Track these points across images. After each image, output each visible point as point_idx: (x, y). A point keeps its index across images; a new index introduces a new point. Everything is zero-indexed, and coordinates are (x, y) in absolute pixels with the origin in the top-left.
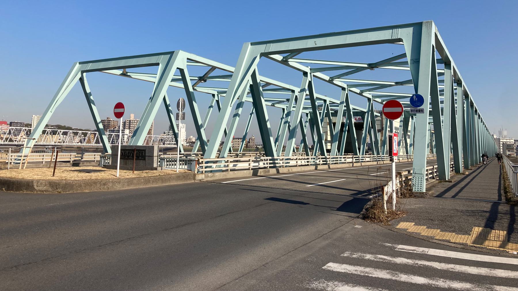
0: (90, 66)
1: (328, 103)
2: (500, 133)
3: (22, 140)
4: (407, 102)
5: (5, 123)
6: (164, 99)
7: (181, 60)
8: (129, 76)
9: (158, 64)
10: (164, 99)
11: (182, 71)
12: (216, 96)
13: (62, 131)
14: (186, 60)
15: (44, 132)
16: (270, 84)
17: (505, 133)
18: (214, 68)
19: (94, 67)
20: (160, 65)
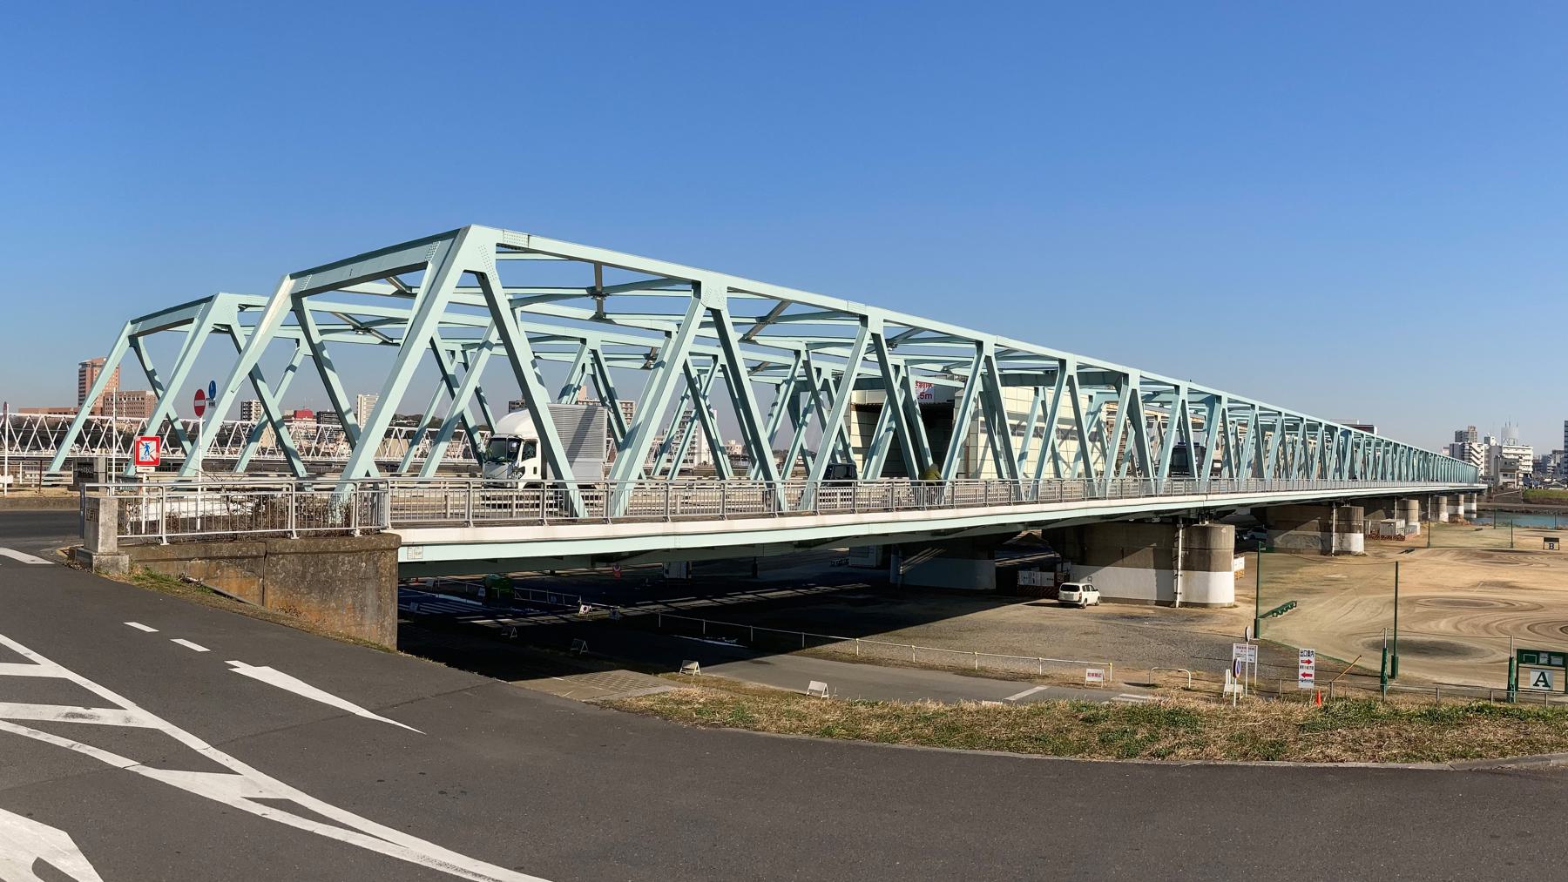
0: (308, 282)
1: (989, 350)
2: (1505, 434)
3: (314, 444)
4: (1446, 453)
5: (307, 414)
6: (686, 366)
7: (480, 247)
8: (610, 321)
9: (423, 266)
10: (686, 366)
11: (716, 313)
12: (902, 370)
13: (405, 429)
14: (494, 248)
15: (388, 434)
16: (923, 330)
17: (1515, 433)
18: (784, 303)
19: (323, 278)
20: (430, 266)
